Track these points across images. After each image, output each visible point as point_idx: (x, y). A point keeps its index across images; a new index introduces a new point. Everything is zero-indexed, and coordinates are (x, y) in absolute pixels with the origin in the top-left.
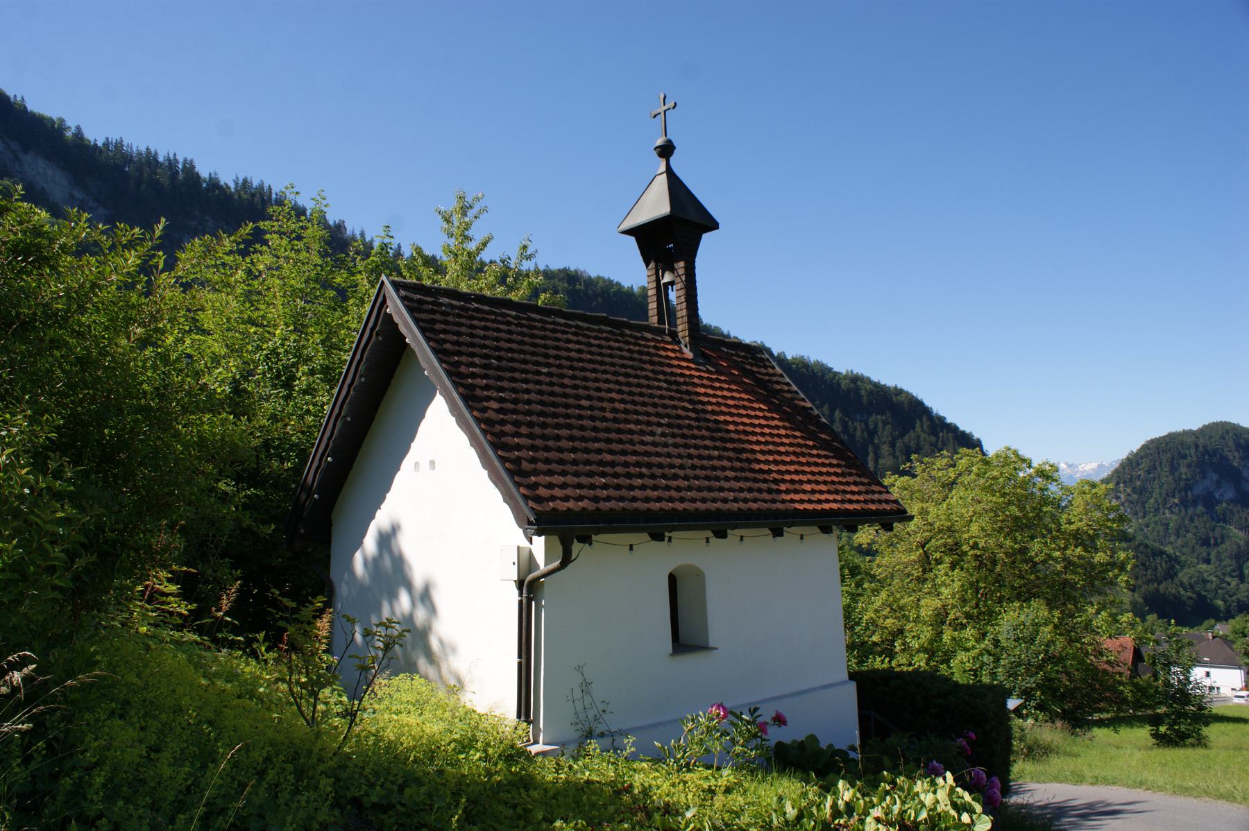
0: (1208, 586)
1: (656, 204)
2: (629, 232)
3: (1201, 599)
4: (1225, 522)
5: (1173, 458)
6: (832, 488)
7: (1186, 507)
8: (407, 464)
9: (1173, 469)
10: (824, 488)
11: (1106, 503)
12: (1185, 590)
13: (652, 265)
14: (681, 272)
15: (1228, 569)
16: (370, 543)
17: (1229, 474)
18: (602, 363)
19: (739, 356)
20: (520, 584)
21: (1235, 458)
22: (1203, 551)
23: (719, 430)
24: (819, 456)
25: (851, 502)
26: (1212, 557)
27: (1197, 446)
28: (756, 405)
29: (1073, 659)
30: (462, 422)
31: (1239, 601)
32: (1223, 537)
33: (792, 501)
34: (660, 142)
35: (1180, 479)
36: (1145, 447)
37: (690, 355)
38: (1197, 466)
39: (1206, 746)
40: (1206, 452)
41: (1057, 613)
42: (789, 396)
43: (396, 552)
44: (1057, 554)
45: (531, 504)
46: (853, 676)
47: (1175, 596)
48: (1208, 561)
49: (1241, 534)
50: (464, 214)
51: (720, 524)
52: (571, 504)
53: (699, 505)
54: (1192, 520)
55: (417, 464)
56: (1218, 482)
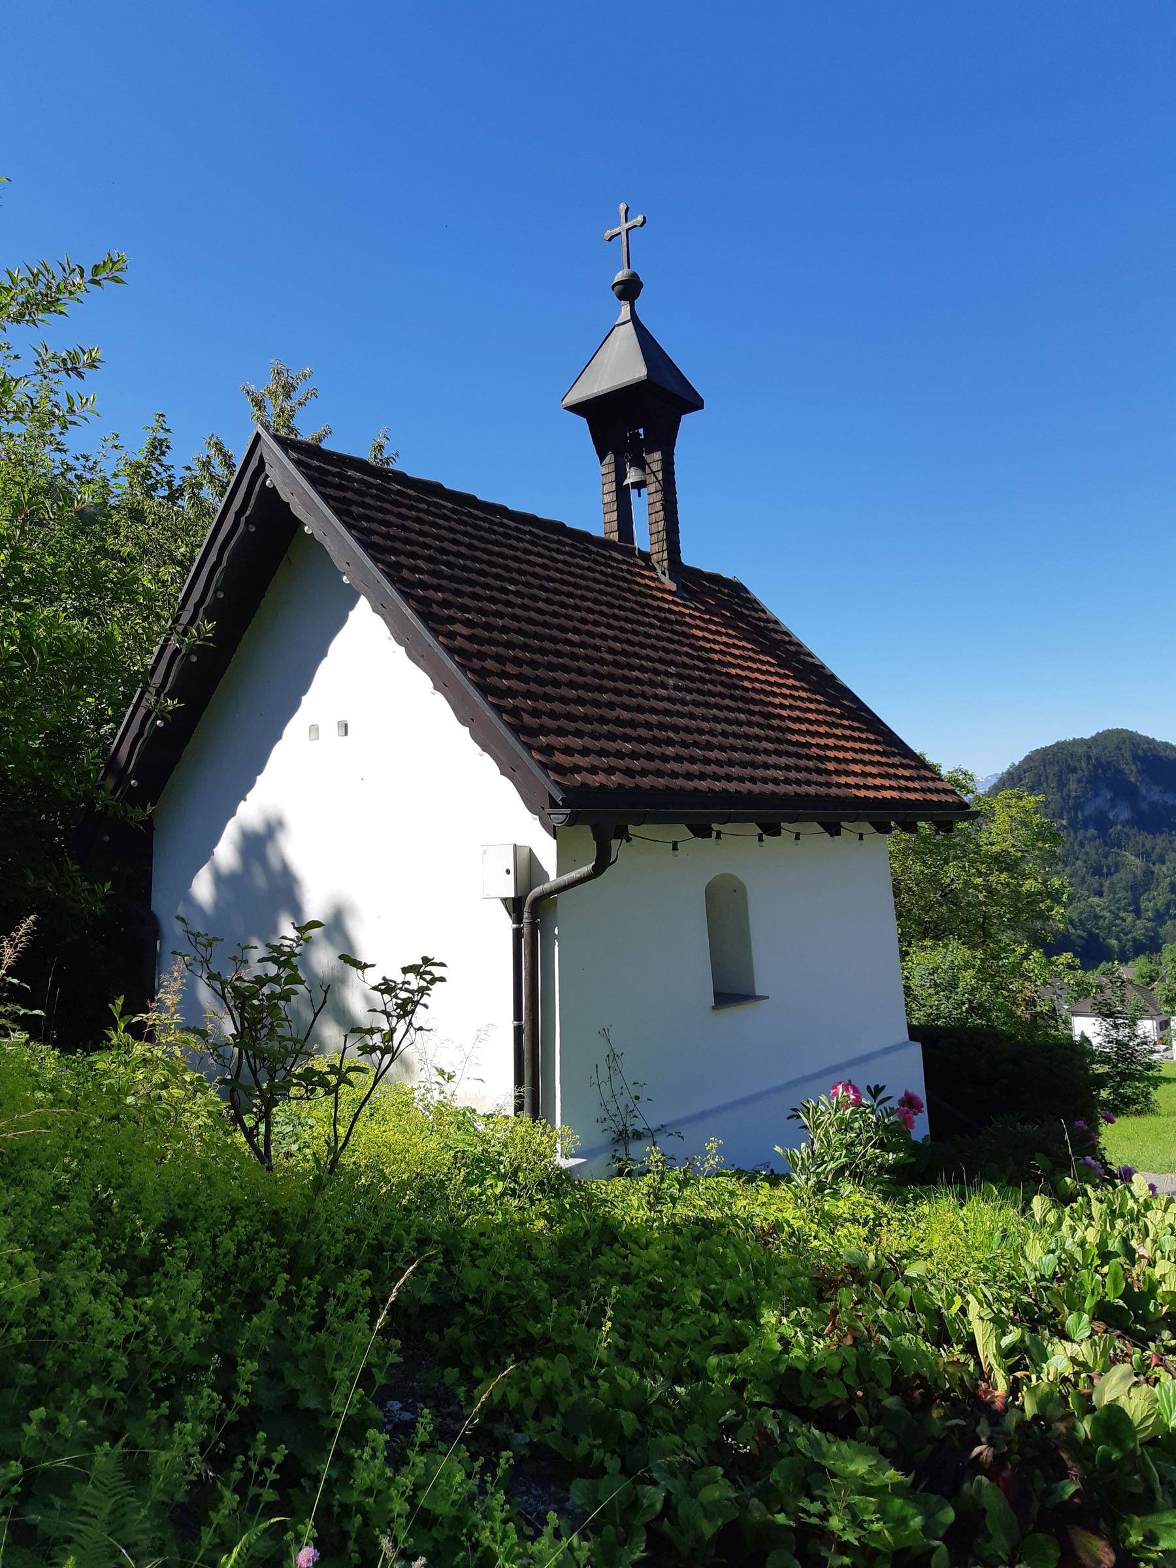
0: (1101, 922)
1: (618, 365)
2: (576, 408)
3: (1093, 937)
4: (1120, 847)
5: (1061, 772)
6: (882, 770)
7: (1076, 830)
8: (295, 729)
9: (1061, 785)
10: (875, 770)
11: (1037, 819)
12: (1075, 927)
13: (610, 458)
14: (656, 467)
15: (1123, 903)
16: (225, 852)
17: (1126, 792)
18: (576, 586)
19: (723, 593)
20: (515, 906)
21: (1132, 773)
22: (1093, 882)
23: (737, 687)
24: (850, 727)
25: (908, 790)
26: (1105, 888)
27: (1089, 758)
28: (762, 657)
29: (999, 1010)
30: (417, 655)
31: (1134, 940)
32: (1117, 865)
33: (847, 785)
34: (620, 276)
35: (1069, 796)
36: (1029, 759)
37: (673, 587)
38: (1088, 782)
39: (1153, 1112)
40: (1099, 764)
41: (979, 954)
42: (793, 648)
43: (275, 864)
44: (979, 880)
45: (553, 776)
46: (915, 1033)
47: (1064, 936)
48: (1100, 894)
49: (1138, 862)
50: (288, 396)
51: (770, 815)
52: (601, 778)
53: (748, 785)
54: (1082, 845)
55: (314, 730)
56: (1112, 800)
